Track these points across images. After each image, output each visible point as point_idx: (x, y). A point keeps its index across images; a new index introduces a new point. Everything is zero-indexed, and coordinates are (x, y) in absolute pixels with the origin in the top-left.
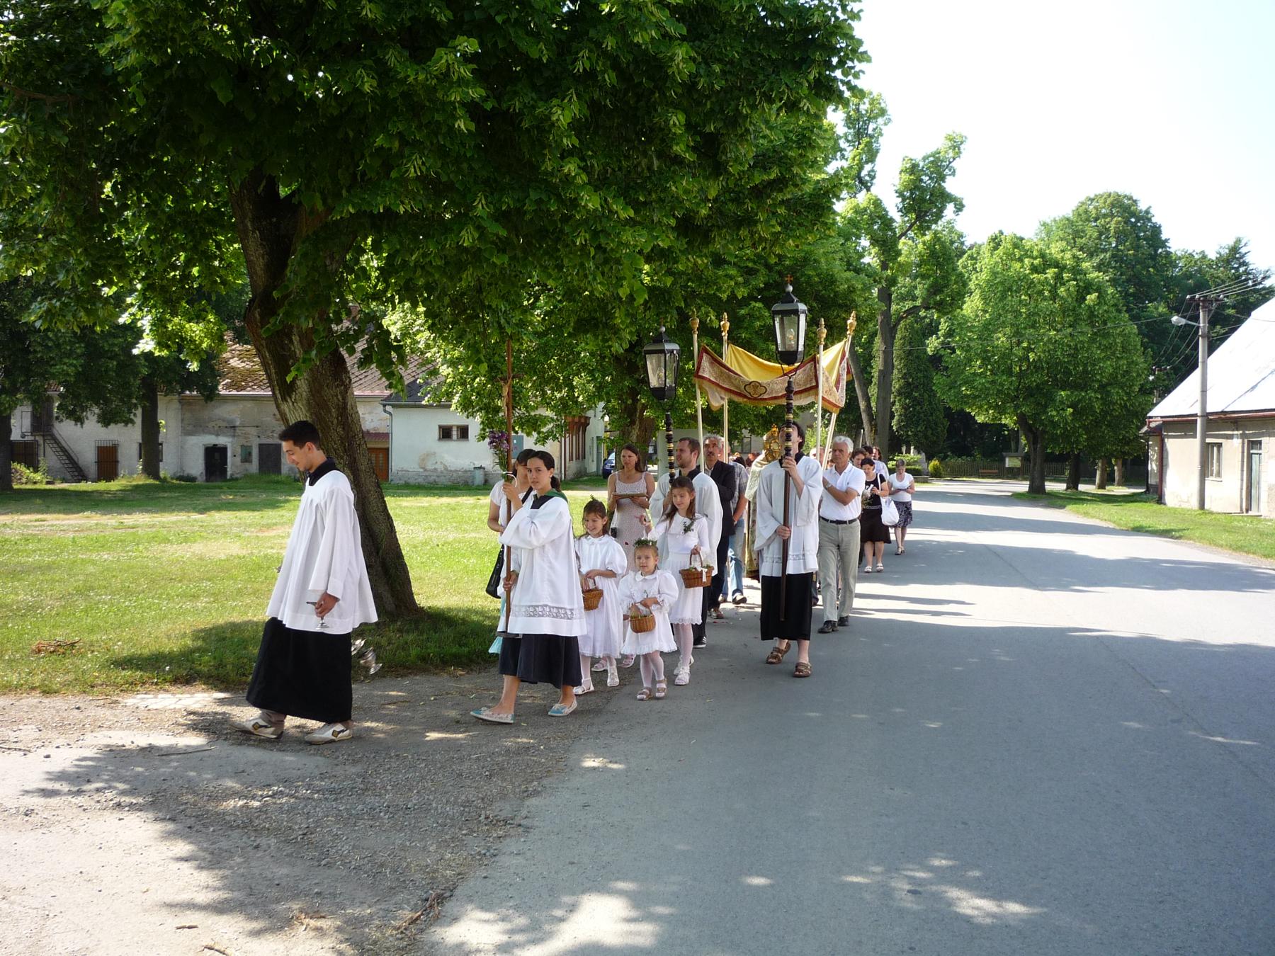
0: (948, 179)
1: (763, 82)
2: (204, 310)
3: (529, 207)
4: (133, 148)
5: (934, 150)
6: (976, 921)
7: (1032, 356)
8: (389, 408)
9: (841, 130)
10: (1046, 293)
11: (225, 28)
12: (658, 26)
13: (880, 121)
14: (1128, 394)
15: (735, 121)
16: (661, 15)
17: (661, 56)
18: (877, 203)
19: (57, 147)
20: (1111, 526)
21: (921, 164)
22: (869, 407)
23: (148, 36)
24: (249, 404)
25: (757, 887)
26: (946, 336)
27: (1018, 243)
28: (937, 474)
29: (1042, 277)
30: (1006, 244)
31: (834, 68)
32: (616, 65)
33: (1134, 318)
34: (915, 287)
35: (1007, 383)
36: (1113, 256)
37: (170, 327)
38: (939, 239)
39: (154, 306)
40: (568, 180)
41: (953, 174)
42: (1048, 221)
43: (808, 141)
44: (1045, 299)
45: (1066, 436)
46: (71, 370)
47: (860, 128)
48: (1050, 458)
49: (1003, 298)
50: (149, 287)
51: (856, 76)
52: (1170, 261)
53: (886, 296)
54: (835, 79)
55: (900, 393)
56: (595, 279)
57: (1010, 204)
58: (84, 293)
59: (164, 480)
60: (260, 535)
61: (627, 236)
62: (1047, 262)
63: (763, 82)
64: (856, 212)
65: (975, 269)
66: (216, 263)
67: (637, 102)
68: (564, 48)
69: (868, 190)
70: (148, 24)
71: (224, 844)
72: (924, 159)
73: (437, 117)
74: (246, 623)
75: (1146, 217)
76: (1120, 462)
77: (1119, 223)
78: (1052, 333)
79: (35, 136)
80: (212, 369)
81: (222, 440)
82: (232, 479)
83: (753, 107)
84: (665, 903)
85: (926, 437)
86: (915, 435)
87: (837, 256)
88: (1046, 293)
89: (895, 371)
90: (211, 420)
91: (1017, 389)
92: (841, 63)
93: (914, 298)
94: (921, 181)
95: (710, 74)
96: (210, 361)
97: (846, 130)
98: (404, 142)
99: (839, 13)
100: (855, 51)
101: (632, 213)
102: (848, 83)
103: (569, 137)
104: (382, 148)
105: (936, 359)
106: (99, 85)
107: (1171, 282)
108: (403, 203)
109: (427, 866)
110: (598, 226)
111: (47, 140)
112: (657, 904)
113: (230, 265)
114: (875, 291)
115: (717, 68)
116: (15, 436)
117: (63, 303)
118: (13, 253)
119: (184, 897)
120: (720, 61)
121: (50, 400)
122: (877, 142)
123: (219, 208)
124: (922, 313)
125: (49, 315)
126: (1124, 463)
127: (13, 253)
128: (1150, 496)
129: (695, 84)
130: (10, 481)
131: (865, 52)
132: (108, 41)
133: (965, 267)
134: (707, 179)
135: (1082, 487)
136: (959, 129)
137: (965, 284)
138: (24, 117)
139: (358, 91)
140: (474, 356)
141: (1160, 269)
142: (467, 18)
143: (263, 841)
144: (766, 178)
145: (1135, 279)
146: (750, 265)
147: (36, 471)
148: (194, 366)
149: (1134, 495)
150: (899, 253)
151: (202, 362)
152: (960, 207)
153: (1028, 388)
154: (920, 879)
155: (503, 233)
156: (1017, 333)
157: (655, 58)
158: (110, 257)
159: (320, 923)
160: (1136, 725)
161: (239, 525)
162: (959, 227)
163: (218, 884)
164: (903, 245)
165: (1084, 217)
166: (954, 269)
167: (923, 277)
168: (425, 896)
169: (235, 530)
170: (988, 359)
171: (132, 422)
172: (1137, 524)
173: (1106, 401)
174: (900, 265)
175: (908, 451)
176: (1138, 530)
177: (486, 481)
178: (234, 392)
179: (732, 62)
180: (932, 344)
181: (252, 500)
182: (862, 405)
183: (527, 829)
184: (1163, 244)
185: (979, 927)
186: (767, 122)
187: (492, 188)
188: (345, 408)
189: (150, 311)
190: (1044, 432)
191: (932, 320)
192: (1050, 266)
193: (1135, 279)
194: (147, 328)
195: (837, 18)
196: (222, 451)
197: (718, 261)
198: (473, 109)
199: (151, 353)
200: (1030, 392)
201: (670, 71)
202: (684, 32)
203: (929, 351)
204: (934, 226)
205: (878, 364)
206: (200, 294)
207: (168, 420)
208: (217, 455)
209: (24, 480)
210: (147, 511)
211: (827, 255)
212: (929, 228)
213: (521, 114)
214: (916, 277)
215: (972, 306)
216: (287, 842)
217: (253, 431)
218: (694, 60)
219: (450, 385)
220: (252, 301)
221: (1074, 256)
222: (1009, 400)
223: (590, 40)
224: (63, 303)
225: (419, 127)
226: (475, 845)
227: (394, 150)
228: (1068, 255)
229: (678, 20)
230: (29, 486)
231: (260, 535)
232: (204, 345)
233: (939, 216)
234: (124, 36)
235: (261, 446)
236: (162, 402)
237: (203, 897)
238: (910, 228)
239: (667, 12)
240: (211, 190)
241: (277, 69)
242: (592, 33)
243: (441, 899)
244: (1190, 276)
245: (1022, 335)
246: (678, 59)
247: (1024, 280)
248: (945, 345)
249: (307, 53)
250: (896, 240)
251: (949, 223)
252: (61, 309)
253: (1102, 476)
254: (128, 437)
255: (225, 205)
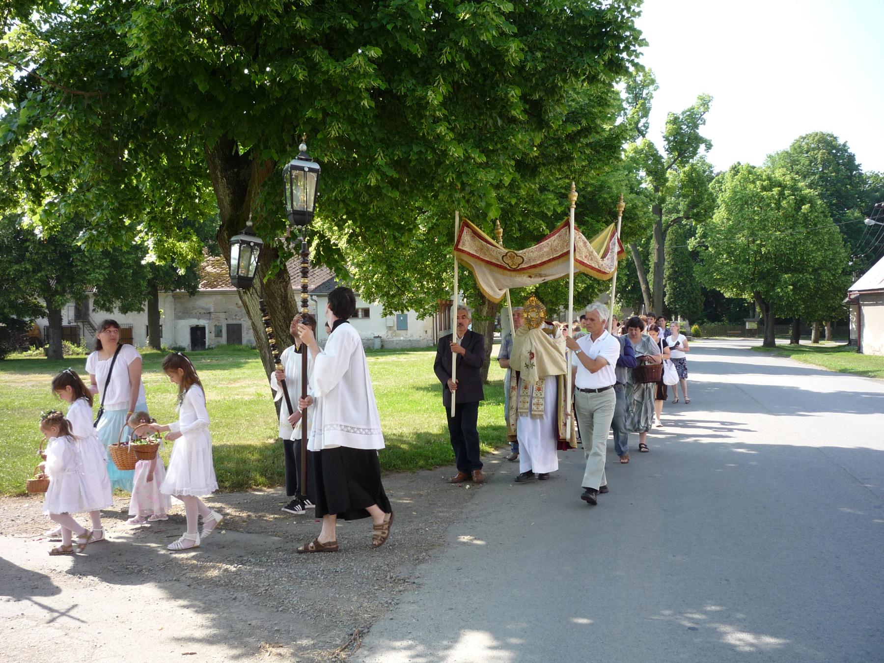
0: (701, 127)
1: (571, 62)
2: (189, 233)
3: (413, 157)
4: (142, 125)
5: (690, 106)
6: (738, 649)
7: (763, 250)
8: (315, 297)
9: (624, 95)
10: (773, 205)
11: (205, 41)
12: (497, 27)
13: (651, 88)
14: (834, 275)
15: (553, 91)
16: (499, 21)
17: (499, 49)
18: (650, 145)
19: (93, 126)
20: (824, 369)
21: (681, 117)
22: (648, 288)
23: (156, 50)
24: (220, 297)
25: (582, 625)
26: (701, 237)
27: (751, 170)
28: (697, 335)
29: (769, 194)
30: (743, 172)
31: (622, 51)
32: (468, 57)
33: (836, 221)
34: (679, 204)
35: (747, 269)
36: (821, 177)
37: (166, 245)
38: (695, 169)
39: (156, 232)
40: (439, 137)
41: (704, 123)
42: (773, 154)
43: (604, 102)
44: (772, 209)
45: (789, 305)
46: (101, 278)
47: (637, 93)
48: (779, 322)
49: (742, 209)
50: (153, 219)
51: (637, 56)
52: (862, 180)
53: (658, 211)
54: (623, 59)
55: (669, 278)
56: (459, 204)
57: (745, 143)
58: (113, 224)
59: (164, 350)
60: (229, 386)
61: (481, 175)
62: (772, 183)
63: (571, 62)
64: (635, 152)
65: (721, 190)
66: (197, 201)
67: (485, 80)
68: (433, 47)
69: (644, 136)
70: (156, 43)
71: (212, 597)
72: (683, 113)
73: (349, 98)
74: (222, 446)
75: (844, 148)
76: (829, 324)
77: (823, 154)
78: (778, 233)
79: (79, 120)
80: (195, 274)
81: (202, 322)
82: (209, 349)
83: (565, 81)
84: (516, 636)
85: (689, 308)
86: (681, 307)
87: (624, 183)
88: (773, 205)
89: (666, 263)
90: (194, 308)
91: (753, 274)
92: (627, 48)
93: (678, 212)
94: (681, 129)
95: (534, 59)
96: (192, 268)
97: (627, 95)
98: (326, 114)
99: (625, 13)
100: (636, 37)
101: (485, 159)
102: (632, 61)
103: (440, 110)
104: (310, 119)
105: (695, 254)
106: (120, 83)
107: (862, 195)
108: (326, 155)
109: (351, 611)
110: (461, 170)
111: (87, 122)
112: (511, 637)
113: (205, 201)
114: (651, 208)
115: (539, 55)
116: (65, 323)
117: (99, 232)
118: (70, 202)
119: (187, 633)
120: (540, 49)
121: (87, 297)
122: (649, 102)
123: (198, 164)
124: (684, 222)
125: (90, 240)
126: (832, 325)
127: (70, 202)
128: (851, 347)
129: (523, 67)
130: (62, 354)
131: (644, 39)
132: (129, 55)
133: (714, 188)
134: (533, 131)
135: (801, 342)
136: (707, 91)
137: (714, 201)
138: (70, 107)
139: (294, 79)
140: (375, 260)
141: (855, 186)
142: (366, 27)
143: (239, 595)
144: (574, 129)
145: (837, 194)
146: (563, 191)
147: (79, 346)
148: (181, 272)
149: (840, 347)
150: (666, 180)
151: (187, 268)
152: (709, 146)
153: (761, 273)
154: (696, 619)
155: (396, 176)
156: (753, 234)
157: (495, 50)
158: (130, 199)
159: (280, 650)
160: (849, 511)
161: (215, 380)
162: (709, 160)
163: (209, 624)
164: (669, 174)
165: (799, 150)
166: (706, 190)
167: (685, 196)
168: (350, 632)
169: (212, 383)
170: (732, 253)
171: (143, 310)
172: (843, 368)
173: (817, 280)
174: (668, 188)
175: (676, 319)
176: (844, 372)
177: (382, 346)
178: (210, 289)
179: (549, 50)
180: (692, 243)
181: (223, 362)
182: (643, 287)
183: (419, 586)
184: (857, 167)
185: (740, 654)
186: (574, 90)
187: (387, 144)
188: (286, 297)
189: (152, 235)
190: (773, 303)
191: (691, 227)
192: (775, 186)
193: (837, 194)
194: (151, 246)
195: (623, 16)
196: (202, 329)
197: (543, 189)
198: (375, 94)
199: (153, 263)
200: (763, 276)
201: (506, 59)
202: (516, 31)
203: (690, 248)
204: (691, 160)
205: (653, 259)
206: (187, 223)
207: (166, 309)
208: (199, 332)
209: (71, 352)
210: (153, 372)
211: (615, 180)
212: (687, 162)
213: (405, 96)
214: (679, 196)
215: (719, 216)
216: (256, 595)
217: (222, 315)
218: (522, 50)
219: (357, 280)
220: (221, 226)
221: (792, 179)
222: (749, 281)
223: (450, 40)
224: (99, 232)
225: (336, 103)
226: (384, 596)
227: (319, 120)
228: (788, 178)
229: (511, 23)
230: (74, 357)
231: (229, 386)
232: (189, 257)
233: (695, 153)
234: (140, 51)
235: (228, 326)
236: (162, 296)
237: (200, 633)
238: (674, 163)
239: (503, 18)
240: (192, 149)
241: (239, 65)
242: (452, 35)
243: (361, 634)
244: (877, 190)
245: (756, 235)
246: (512, 50)
247: (756, 196)
248: (701, 244)
249: (257, 56)
250: (664, 172)
251: (701, 158)
252: (98, 236)
253: (816, 334)
254: (138, 321)
255: (202, 161)
